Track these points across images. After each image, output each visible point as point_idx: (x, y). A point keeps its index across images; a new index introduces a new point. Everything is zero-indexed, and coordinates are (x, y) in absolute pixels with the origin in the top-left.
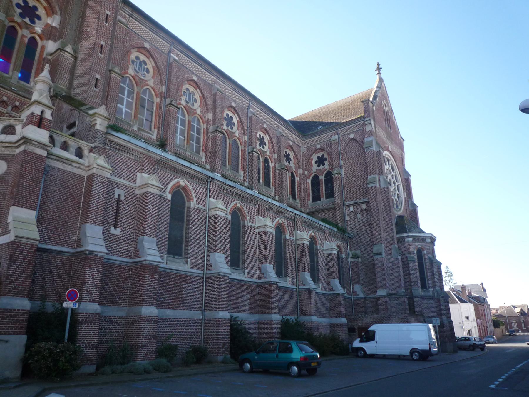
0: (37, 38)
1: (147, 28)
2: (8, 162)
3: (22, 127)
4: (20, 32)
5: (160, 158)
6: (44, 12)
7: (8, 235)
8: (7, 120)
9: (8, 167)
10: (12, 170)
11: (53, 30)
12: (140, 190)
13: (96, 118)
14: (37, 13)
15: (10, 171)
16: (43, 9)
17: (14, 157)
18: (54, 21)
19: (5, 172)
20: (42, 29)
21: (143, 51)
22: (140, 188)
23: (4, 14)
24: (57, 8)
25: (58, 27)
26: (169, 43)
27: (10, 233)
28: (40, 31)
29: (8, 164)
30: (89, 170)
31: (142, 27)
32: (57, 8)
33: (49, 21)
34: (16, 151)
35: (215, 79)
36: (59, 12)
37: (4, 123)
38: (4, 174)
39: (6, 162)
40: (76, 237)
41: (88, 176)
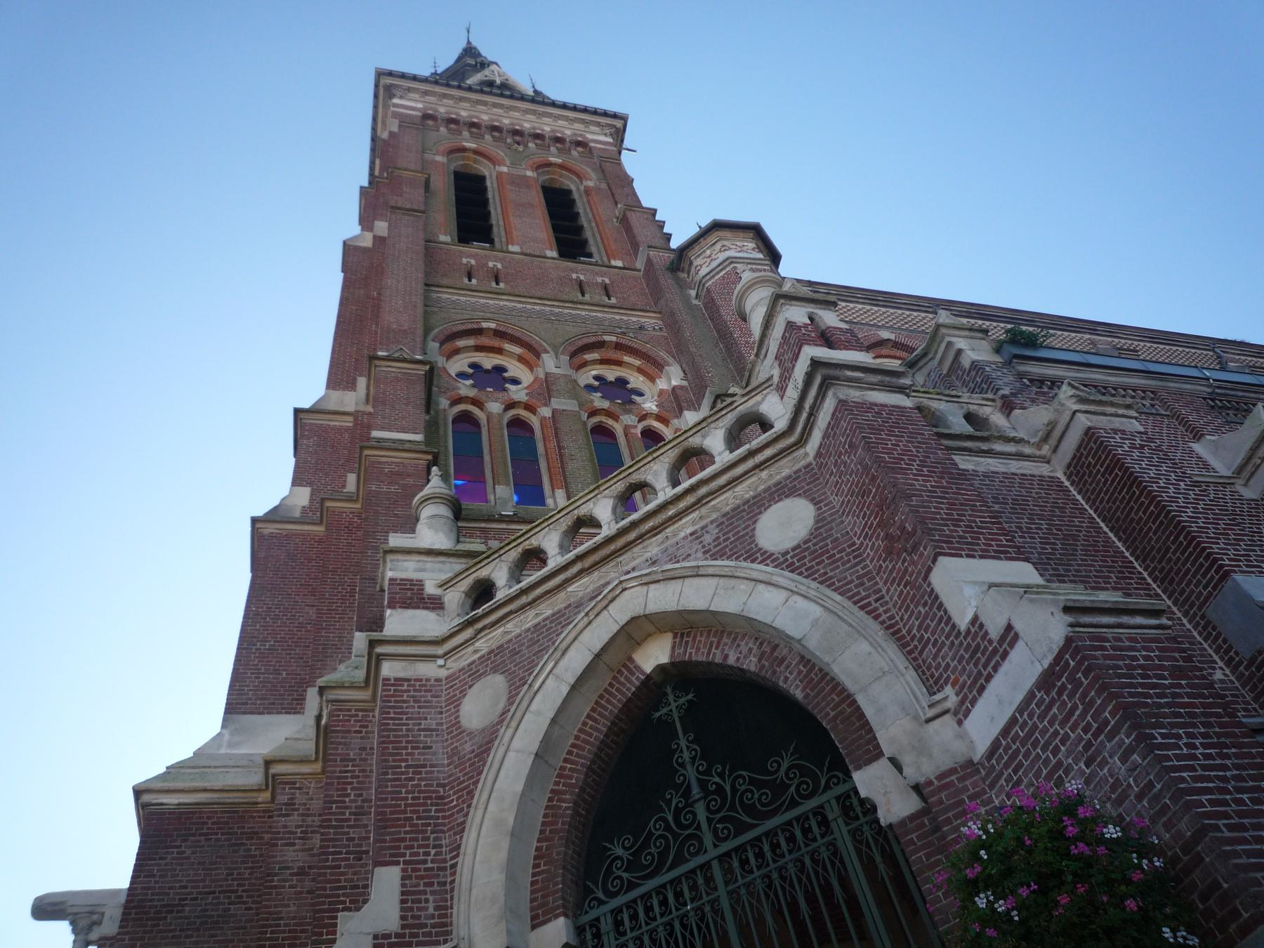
0: (656, 425)
1: (863, 303)
2: (805, 492)
3: (779, 398)
4: (618, 428)
5: (1209, 390)
6: (641, 378)
7: (1020, 645)
8: (724, 412)
9: (815, 504)
10: (836, 500)
11: (679, 392)
12: (1252, 482)
13: (948, 339)
14: (629, 386)
15: (830, 509)
16: (636, 374)
17: (813, 469)
18: (674, 377)
19: (817, 522)
20: (656, 403)
21: (884, 351)
22: (1245, 474)
23: (573, 399)
24: (663, 354)
25: (685, 383)
26: (930, 310)
27: (1017, 637)
28: (654, 408)
29: (806, 497)
30: (1055, 450)
31: (852, 305)
32: (663, 354)
33: (662, 384)
34: (807, 454)
35: (1087, 336)
36: (670, 360)
37: (721, 425)
38: (817, 529)
39: (800, 495)
40: (1221, 668)
41: (1069, 466)
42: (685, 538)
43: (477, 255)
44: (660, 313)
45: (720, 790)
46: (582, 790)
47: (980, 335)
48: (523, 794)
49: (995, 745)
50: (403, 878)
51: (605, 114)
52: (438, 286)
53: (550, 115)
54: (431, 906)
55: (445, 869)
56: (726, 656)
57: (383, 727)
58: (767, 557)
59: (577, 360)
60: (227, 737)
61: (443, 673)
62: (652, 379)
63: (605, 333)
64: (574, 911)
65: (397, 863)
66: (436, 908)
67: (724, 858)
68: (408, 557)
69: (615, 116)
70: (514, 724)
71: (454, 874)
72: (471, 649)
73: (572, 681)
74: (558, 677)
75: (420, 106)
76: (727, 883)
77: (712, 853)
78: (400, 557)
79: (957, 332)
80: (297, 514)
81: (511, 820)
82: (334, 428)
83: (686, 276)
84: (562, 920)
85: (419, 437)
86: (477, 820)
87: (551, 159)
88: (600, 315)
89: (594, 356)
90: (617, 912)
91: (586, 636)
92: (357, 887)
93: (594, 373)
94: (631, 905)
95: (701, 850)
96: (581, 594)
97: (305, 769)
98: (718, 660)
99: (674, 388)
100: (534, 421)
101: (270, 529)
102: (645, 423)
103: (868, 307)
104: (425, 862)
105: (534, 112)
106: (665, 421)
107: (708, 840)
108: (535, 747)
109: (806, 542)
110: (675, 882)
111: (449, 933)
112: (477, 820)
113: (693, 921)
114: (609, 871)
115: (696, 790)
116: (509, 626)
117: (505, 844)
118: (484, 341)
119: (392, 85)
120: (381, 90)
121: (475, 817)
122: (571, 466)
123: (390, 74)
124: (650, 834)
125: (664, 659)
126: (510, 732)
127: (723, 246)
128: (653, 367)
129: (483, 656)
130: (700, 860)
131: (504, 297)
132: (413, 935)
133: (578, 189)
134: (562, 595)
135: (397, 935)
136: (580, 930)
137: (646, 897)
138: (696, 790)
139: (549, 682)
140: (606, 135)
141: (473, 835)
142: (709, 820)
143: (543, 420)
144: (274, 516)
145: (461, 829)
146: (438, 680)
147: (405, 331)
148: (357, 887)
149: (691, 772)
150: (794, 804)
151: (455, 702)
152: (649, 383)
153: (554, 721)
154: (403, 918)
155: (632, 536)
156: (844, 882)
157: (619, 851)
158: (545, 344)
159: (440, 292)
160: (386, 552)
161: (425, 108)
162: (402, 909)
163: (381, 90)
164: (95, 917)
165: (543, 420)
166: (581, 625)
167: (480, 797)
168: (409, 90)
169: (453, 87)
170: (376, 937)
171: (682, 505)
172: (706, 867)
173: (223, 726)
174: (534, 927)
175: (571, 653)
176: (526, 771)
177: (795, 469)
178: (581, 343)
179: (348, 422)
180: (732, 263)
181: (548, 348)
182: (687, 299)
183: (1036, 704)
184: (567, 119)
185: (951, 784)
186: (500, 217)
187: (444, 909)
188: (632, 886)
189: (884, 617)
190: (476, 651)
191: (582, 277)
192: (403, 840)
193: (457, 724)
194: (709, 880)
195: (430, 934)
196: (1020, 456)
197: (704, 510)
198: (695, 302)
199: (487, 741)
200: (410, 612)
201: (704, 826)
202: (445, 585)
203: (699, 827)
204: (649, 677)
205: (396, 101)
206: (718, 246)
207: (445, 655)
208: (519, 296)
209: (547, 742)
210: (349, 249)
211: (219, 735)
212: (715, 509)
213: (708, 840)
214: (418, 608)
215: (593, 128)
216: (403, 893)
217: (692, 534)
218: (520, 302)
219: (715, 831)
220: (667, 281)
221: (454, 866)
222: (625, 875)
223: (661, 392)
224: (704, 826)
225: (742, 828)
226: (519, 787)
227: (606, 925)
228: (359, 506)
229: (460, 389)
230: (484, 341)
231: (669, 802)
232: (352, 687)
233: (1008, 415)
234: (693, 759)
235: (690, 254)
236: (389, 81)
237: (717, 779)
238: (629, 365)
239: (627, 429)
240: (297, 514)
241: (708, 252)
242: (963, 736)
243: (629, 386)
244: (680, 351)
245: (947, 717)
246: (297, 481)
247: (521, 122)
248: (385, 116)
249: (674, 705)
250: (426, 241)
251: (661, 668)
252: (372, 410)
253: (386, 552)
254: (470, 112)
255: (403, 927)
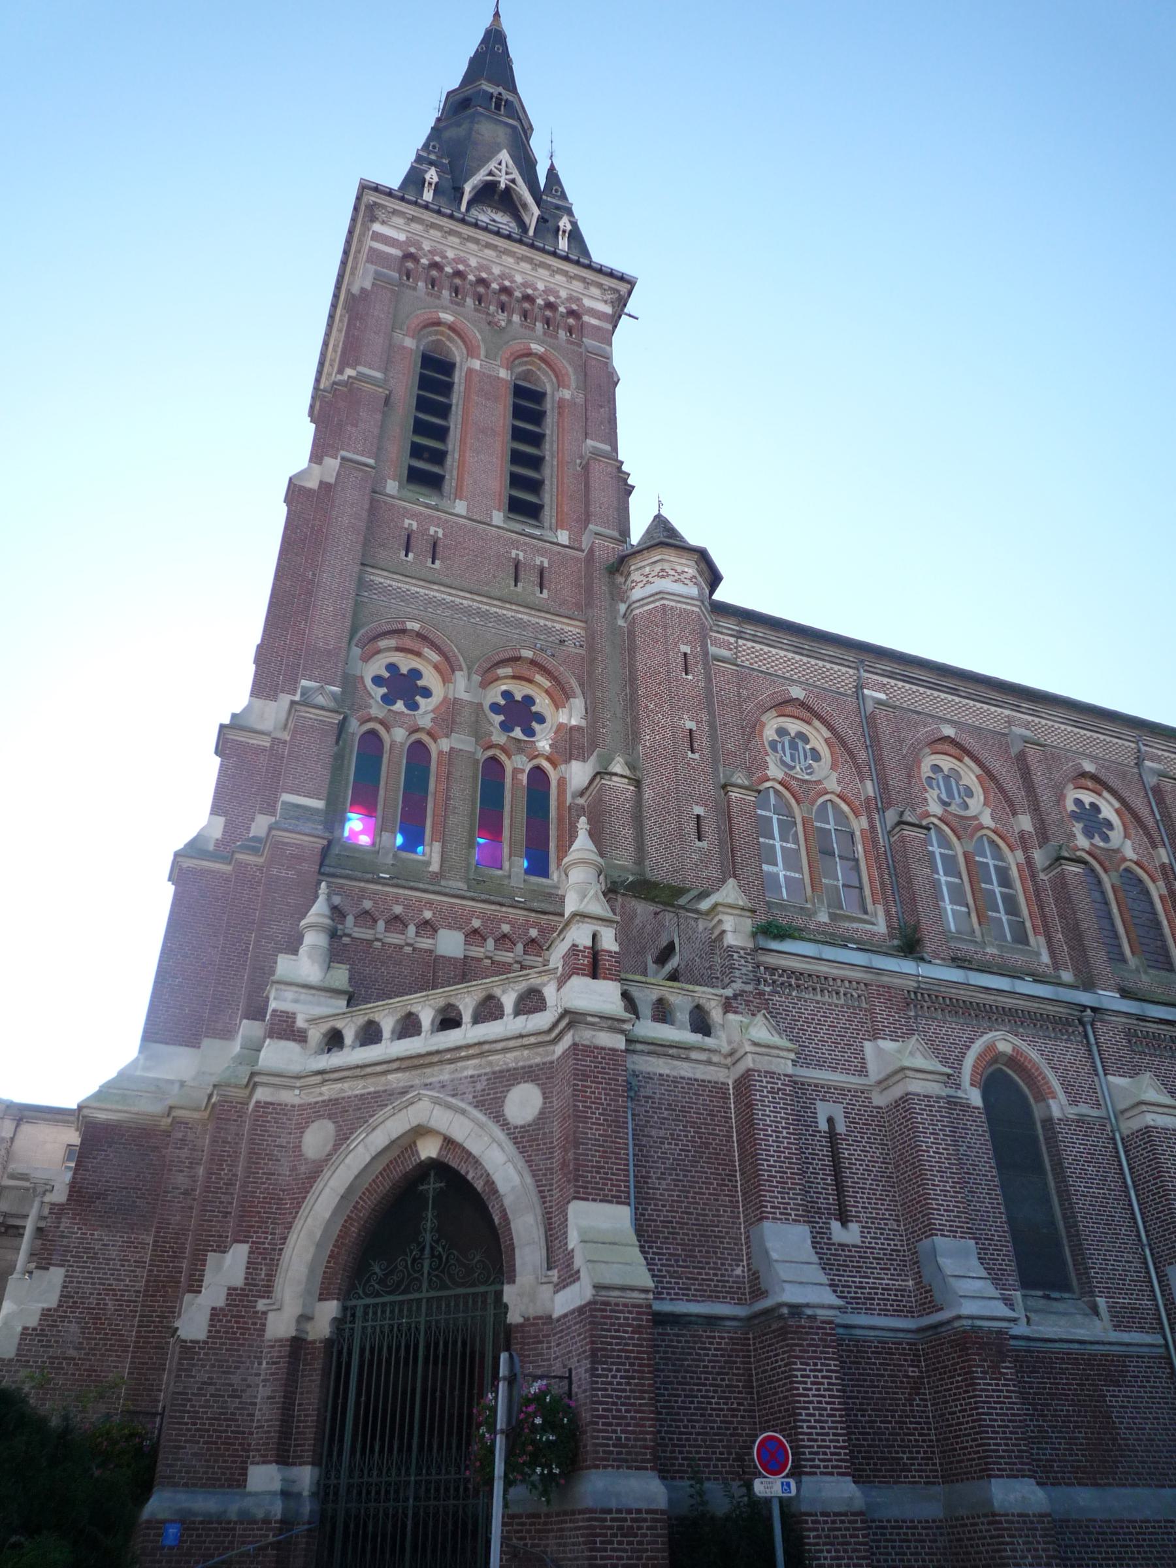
6: (547, 701)
7: (577, 1284)
11: (576, 734)
13: (720, 917)
16: (544, 695)
18: (573, 715)
19: (541, 1113)
26: (853, 665)
28: (547, 748)
32: (574, 682)
33: (563, 717)
42: (466, 1077)
43: (421, 514)
44: (586, 622)
45: (440, 1257)
46: (366, 1222)
47: (749, 914)
48: (329, 1220)
49: (565, 1316)
50: (250, 1253)
51: (611, 274)
52: (373, 567)
53: (548, 267)
54: (263, 1273)
55: (274, 1250)
56: (467, 1172)
57: (252, 1141)
58: (504, 1124)
59: (490, 676)
60: (141, 1062)
61: (297, 1101)
62: (557, 707)
63: (524, 647)
64: (345, 1295)
65: (247, 1242)
66: (267, 1275)
67: (429, 1300)
68: (288, 988)
69: (622, 278)
70: (333, 1168)
71: (280, 1255)
72: (317, 1090)
73: (374, 1154)
74: (366, 1146)
75: (402, 237)
76: (427, 1315)
77: (424, 1295)
78: (283, 987)
79: (729, 911)
80: (211, 847)
81: (318, 1236)
82: (251, 746)
83: (623, 580)
84: (335, 1302)
85: (319, 804)
86: (299, 1227)
87: (533, 346)
88: (525, 617)
89: (508, 671)
90: (367, 1306)
91: (389, 1123)
92: (221, 1236)
93: (504, 688)
94: (375, 1306)
95: (419, 1290)
96: (395, 1085)
97: (196, 1115)
98: (463, 1172)
99: (572, 728)
100: (433, 748)
101: (188, 863)
102: (535, 762)
103: (790, 655)
104: (264, 1243)
105: (530, 260)
106: (554, 765)
107: (425, 1285)
108: (342, 1191)
109: (529, 1125)
110: (402, 1303)
111: (271, 1292)
112: (299, 1227)
113: (404, 1329)
114: (368, 1280)
115: (427, 1251)
116: (346, 1085)
117: (312, 1250)
118: (407, 642)
119: (375, 203)
120: (363, 208)
121: (298, 1224)
122: (452, 820)
123: (376, 189)
124: (396, 1267)
125: (434, 1154)
126: (329, 1173)
127: (663, 570)
128: (561, 695)
129: (323, 1101)
130: (416, 1296)
131: (435, 587)
132: (251, 1291)
133: (553, 395)
134: (383, 1079)
135: (242, 1289)
136: (345, 1309)
137: (384, 1304)
138: (427, 1251)
139: (360, 1147)
140: (606, 302)
141: (295, 1236)
142: (429, 1273)
143: (440, 753)
144: (194, 849)
145: (289, 1227)
146: (293, 1106)
147: (329, 651)
148: (221, 1236)
149: (428, 1237)
150: (473, 1285)
151: (302, 1128)
152: (552, 708)
153: (357, 1177)
154: (246, 1279)
155: (435, 1059)
156: (483, 1341)
157: (377, 1270)
158: (461, 659)
159: (373, 574)
160: (274, 982)
161: (409, 242)
162: (247, 1273)
163: (363, 208)
164: (48, 1187)
165: (440, 753)
166: (387, 1115)
167: (303, 1212)
168: (395, 212)
169: (444, 215)
170: (229, 1289)
171: (471, 1052)
172: (419, 1301)
173: (140, 1052)
174: (320, 1300)
175: (378, 1132)
176: (333, 1206)
177: (545, 1060)
178: (497, 658)
179: (266, 742)
180: (662, 598)
181: (464, 665)
182: (614, 612)
183: (951, 903)
184: (565, 273)
185: (537, 1324)
186: (458, 444)
187: (271, 1276)
188: (378, 1295)
189: (548, 1204)
190: (321, 1094)
191: (521, 556)
192: (253, 1227)
193: (298, 1147)
194: (419, 1308)
195: (260, 1291)
196: (709, 1062)
197: (484, 1061)
198: (621, 622)
199: (316, 1172)
200: (283, 1043)
201: (426, 1275)
202: (312, 1021)
203: (422, 1275)
204: (422, 1162)
205: (377, 227)
206: (658, 568)
207: (301, 1088)
208: (450, 587)
209: (350, 1189)
210: (296, 493)
211: (137, 1059)
212: (490, 1064)
213: (425, 1285)
214: (288, 1039)
215: (595, 291)
216: (248, 1263)
217: (472, 1077)
218: (450, 594)
219: (430, 1281)
220: (601, 587)
221: (281, 1250)
222: (377, 1286)
223: (561, 726)
224: (426, 1275)
225: (444, 1287)
226: (327, 1215)
227: (359, 1313)
228: (261, 860)
229: (371, 707)
230: (407, 642)
231: (411, 1251)
232: (236, 1086)
233: (725, 1013)
234: (432, 1229)
235: (632, 562)
236: (371, 197)
237: (440, 1249)
238: (539, 685)
239: (516, 771)
240: (211, 847)
241: (647, 569)
242: (552, 1300)
243: (534, 709)
244: (589, 686)
245: (551, 1286)
246: (216, 810)
247: (513, 273)
248: (363, 234)
249: (432, 1186)
250: (362, 564)
251: (430, 1159)
252: (288, 738)
253: (274, 982)
254: (457, 252)
255: (246, 1284)
